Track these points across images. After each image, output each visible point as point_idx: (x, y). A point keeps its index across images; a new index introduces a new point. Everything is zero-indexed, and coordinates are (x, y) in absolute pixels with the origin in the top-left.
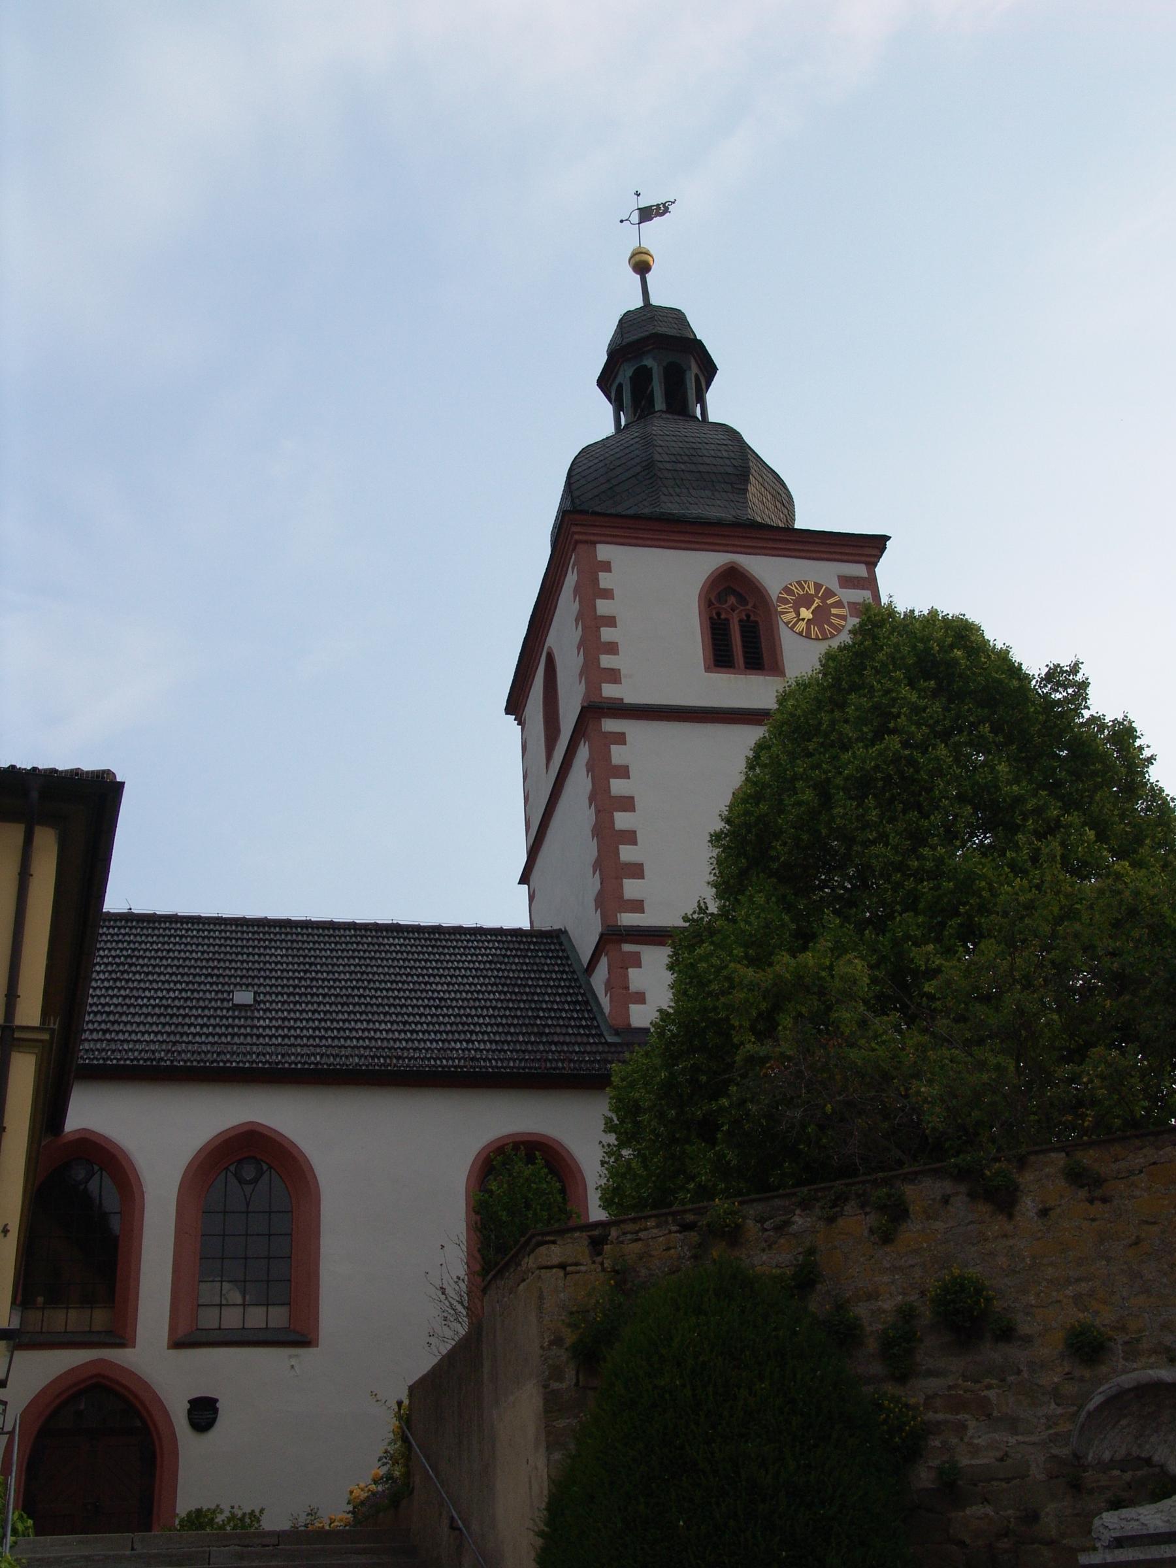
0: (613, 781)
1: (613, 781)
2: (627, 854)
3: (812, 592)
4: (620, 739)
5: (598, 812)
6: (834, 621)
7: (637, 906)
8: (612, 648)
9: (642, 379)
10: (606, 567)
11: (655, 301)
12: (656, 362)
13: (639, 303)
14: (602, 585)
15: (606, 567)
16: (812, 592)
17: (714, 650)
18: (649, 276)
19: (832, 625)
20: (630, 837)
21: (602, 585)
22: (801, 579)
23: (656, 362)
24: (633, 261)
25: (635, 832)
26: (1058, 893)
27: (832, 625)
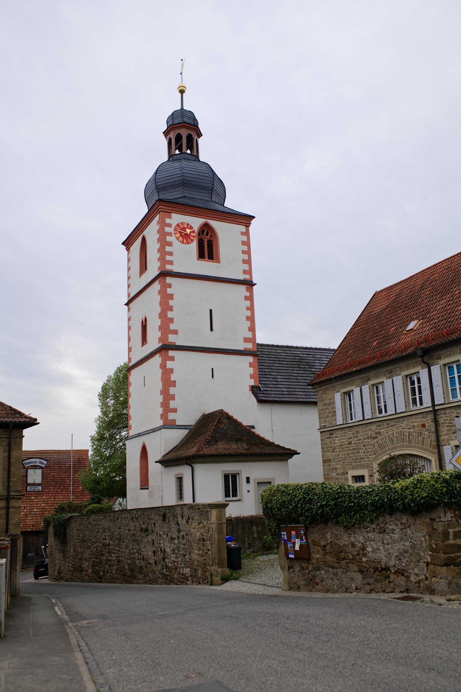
0: (167, 237)
1: (167, 237)
2: (169, 291)
3: (186, 227)
4: (172, 359)
5: (161, 245)
6: (192, 238)
7: (171, 263)
8: (171, 254)
9: (179, 138)
10: (170, 286)
11: (185, 108)
12: (183, 131)
13: (179, 108)
14: (171, 407)
15: (170, 286)
16: (186, 227)
17: (199, 246)
18: (184, 94)
19: (191, 239)
20: (172, 320)
21: (171, 407)
22: (183, 222)
23: (183, 131)
24: (179, 89)
25: (173, 369)
26: (321, 649)
27: (191, 239)
